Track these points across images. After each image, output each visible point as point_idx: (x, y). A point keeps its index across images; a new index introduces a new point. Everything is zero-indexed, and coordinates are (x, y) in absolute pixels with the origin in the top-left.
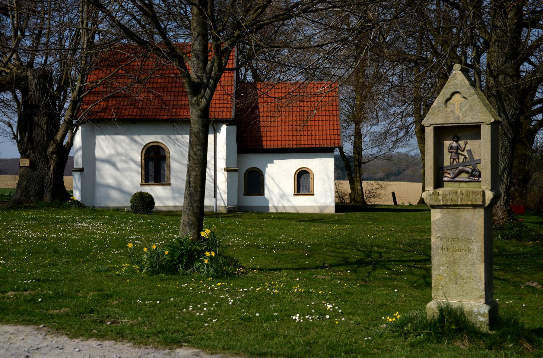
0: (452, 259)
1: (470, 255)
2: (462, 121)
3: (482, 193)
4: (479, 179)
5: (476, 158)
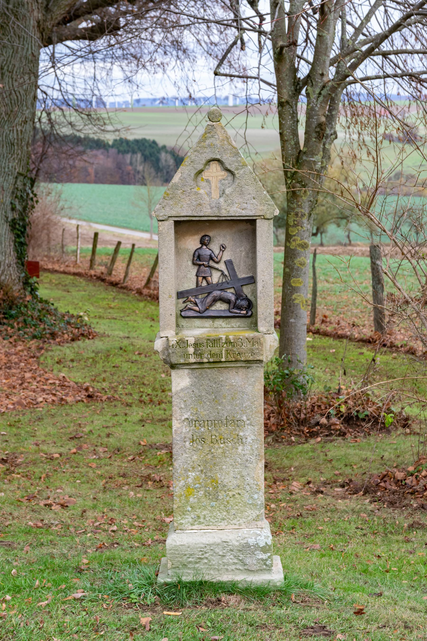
0: (209, 457)
1: (240, 448)
2: (224, 213)
4: (247, 313)
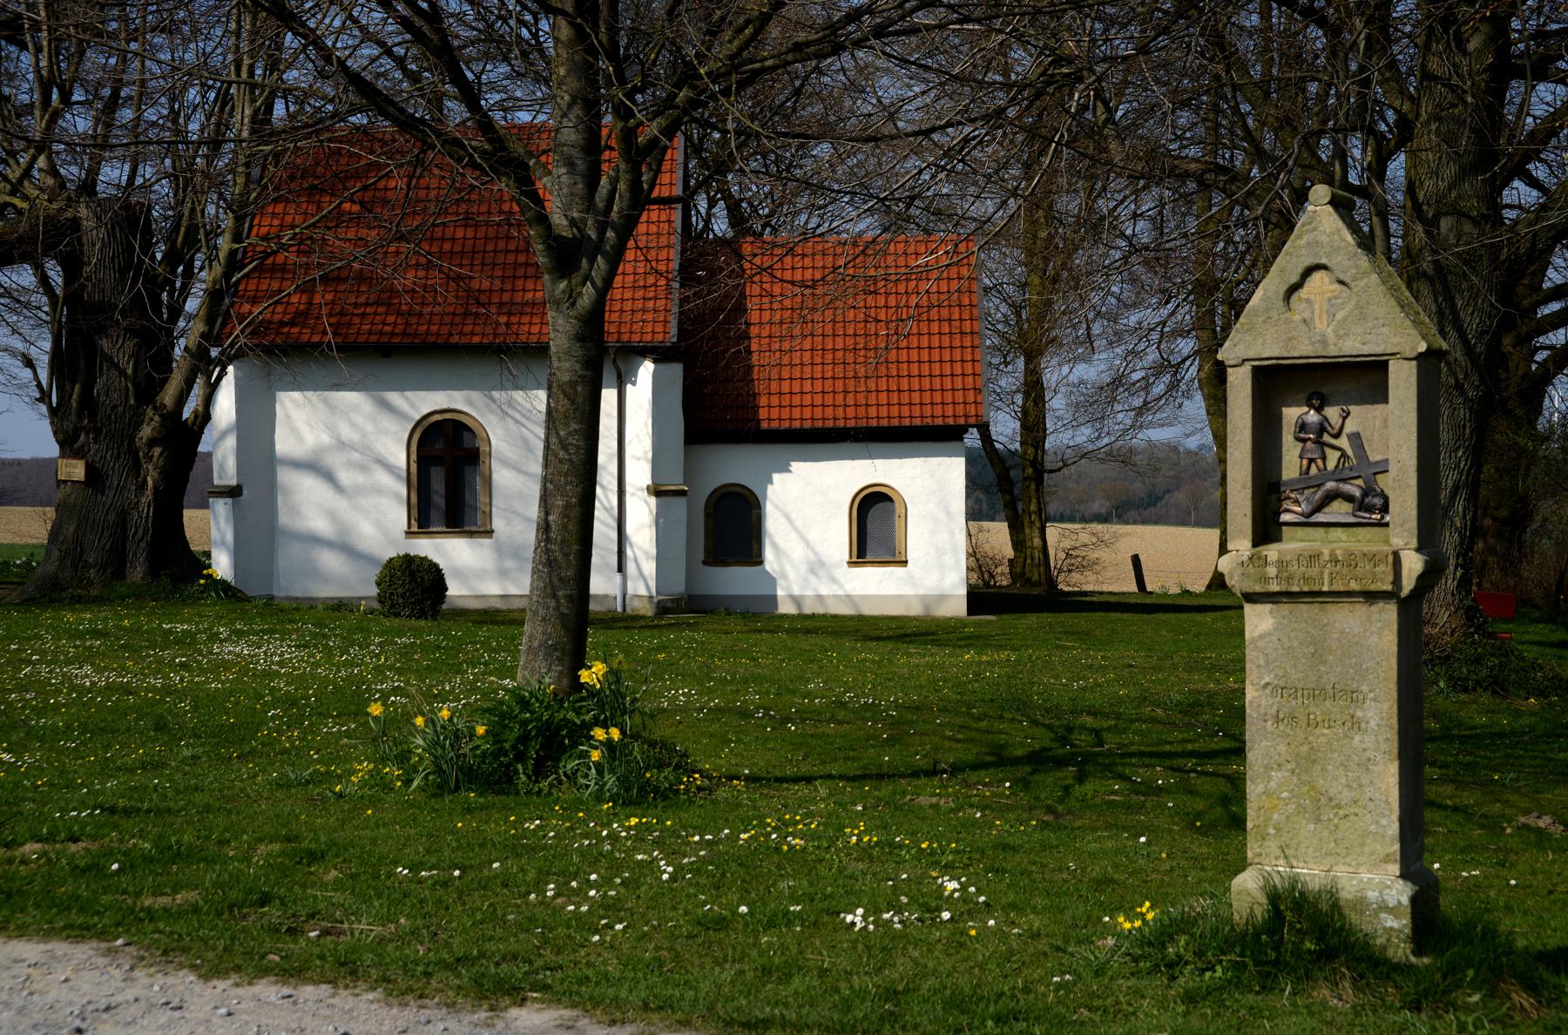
0: (1305, 748)
1: (1357, 738)
2: (1333, 351)
3: (1391, 558)
4: (1382, 518)
5: (1374, 457)
